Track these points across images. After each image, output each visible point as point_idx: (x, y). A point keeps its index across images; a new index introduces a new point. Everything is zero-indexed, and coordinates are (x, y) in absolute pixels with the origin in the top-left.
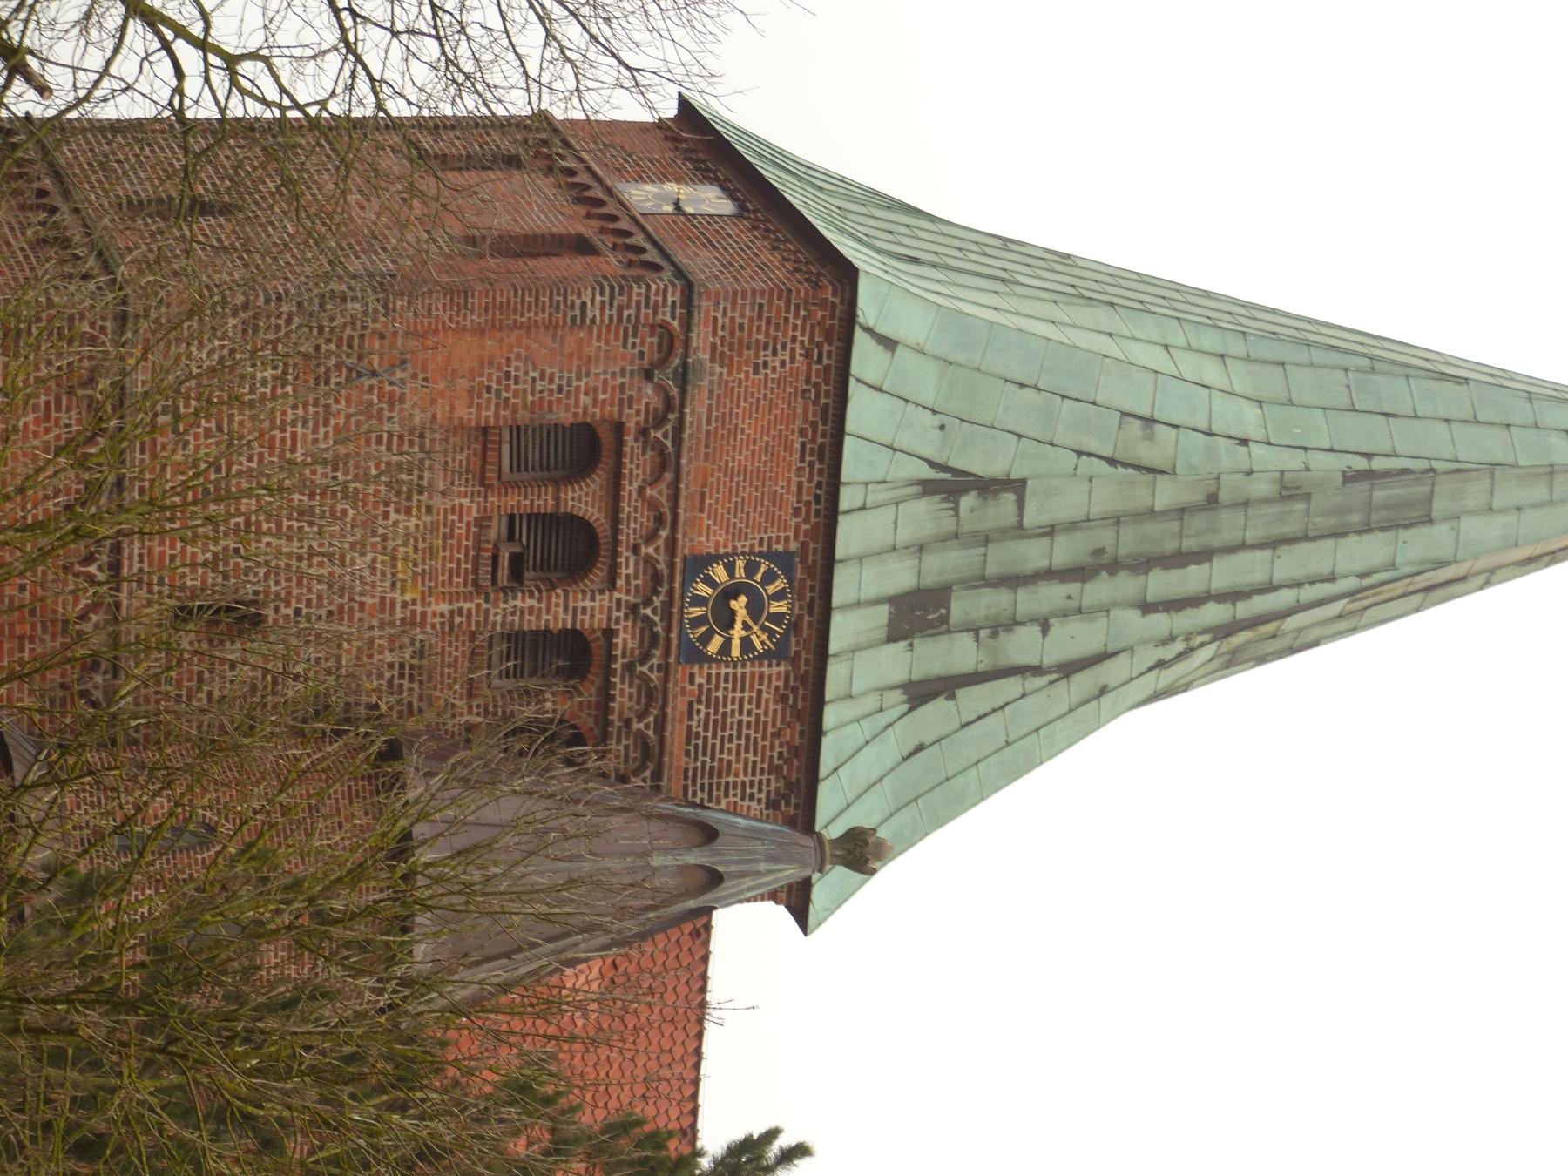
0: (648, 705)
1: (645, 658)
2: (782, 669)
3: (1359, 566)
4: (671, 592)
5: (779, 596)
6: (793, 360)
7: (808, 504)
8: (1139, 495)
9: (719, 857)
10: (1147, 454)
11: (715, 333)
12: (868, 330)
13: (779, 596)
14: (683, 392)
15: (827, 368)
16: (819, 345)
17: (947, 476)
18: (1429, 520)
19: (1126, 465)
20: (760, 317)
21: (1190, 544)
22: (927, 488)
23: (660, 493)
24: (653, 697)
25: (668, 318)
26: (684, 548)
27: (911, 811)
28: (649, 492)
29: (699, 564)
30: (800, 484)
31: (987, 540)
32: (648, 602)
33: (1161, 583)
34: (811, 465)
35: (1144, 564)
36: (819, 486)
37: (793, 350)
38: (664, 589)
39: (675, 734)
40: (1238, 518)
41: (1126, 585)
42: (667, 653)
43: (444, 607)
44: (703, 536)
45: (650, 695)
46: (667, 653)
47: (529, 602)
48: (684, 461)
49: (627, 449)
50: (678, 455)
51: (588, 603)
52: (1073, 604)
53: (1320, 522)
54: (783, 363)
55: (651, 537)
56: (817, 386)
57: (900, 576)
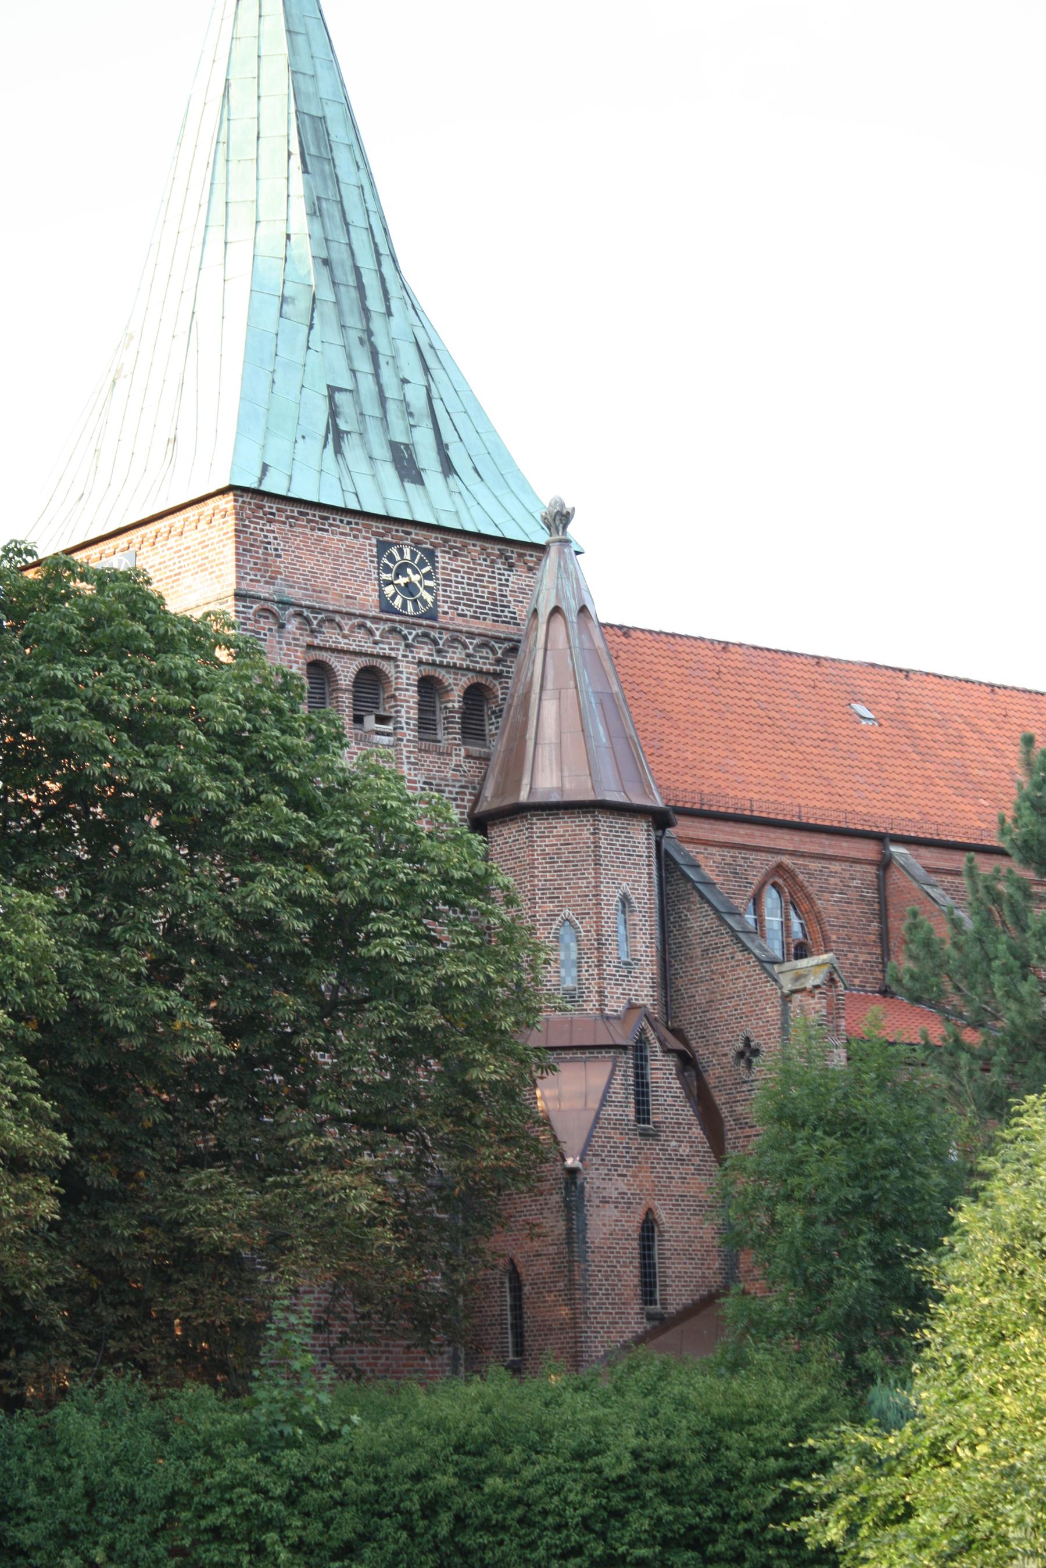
0: (460, 642)
1: (435, 642)
2: (439, 554)
3: (354, 168)
4: (401, 622)
5: (401, 552)
6: (273, 532)
7: (352, 529)
8: (327, 310)
9: (571, 607)
10: (304, 303)
11: (258, 581)
12: (261, 481)
13: (401, 552)
14: (292, 604)
15: (278, 510)
16: (265, 514)
17: (330, 436)
18: (323, 118)
19: (312, 318)
20: (250, 551)
21: (352, 280)
22: (338, 451)
23: (347, 624)
24: (456, 639)
25: (251, 611)
26: (375, 612)
27: (508, 477)
28: (346, 632)
29: (386, 606)
30: (342, 534)
31: (361, 414)
32: (405, 638)
33: (375, 303)
34: (331, 525)
35: (366, 312)
36: (341, 521)
37: (268, 531)
38: (397, 625)
39: (476, 626)
40: (333, 245)
41: (377, 324)
42: (433, 627)
43: (405, 767)
44: (368, 600)
45: (455, 640)
46: (433, 627)
47: (403, 713)
48: (331, 608)
49: (321, 644)
50: (328, 611)
51: (404, 676)
52: (391, 361)
53: (331, 193)
54: (275, 538)
55: (371, 632)
56: (288, 517)
57: (388, 473)
